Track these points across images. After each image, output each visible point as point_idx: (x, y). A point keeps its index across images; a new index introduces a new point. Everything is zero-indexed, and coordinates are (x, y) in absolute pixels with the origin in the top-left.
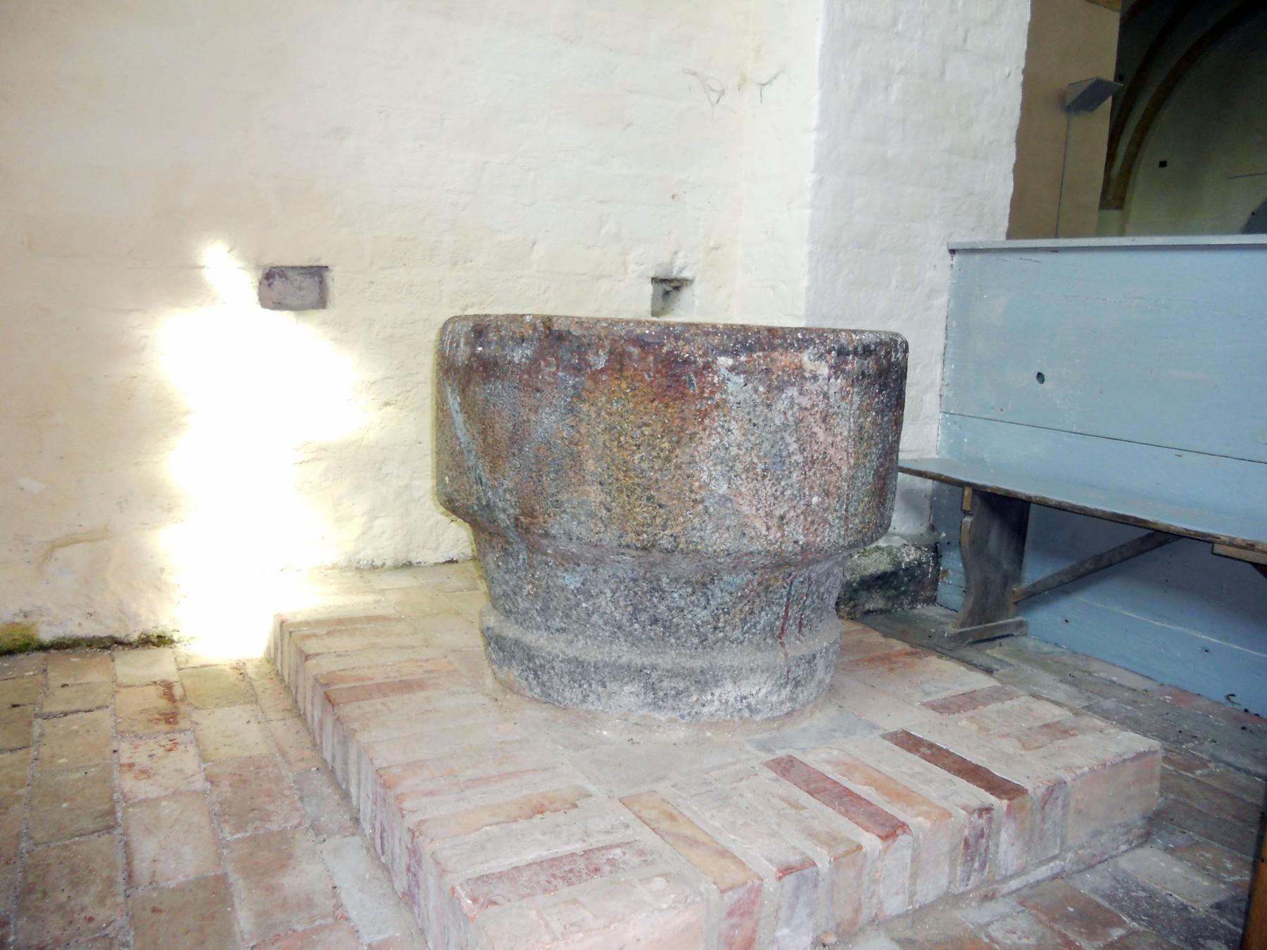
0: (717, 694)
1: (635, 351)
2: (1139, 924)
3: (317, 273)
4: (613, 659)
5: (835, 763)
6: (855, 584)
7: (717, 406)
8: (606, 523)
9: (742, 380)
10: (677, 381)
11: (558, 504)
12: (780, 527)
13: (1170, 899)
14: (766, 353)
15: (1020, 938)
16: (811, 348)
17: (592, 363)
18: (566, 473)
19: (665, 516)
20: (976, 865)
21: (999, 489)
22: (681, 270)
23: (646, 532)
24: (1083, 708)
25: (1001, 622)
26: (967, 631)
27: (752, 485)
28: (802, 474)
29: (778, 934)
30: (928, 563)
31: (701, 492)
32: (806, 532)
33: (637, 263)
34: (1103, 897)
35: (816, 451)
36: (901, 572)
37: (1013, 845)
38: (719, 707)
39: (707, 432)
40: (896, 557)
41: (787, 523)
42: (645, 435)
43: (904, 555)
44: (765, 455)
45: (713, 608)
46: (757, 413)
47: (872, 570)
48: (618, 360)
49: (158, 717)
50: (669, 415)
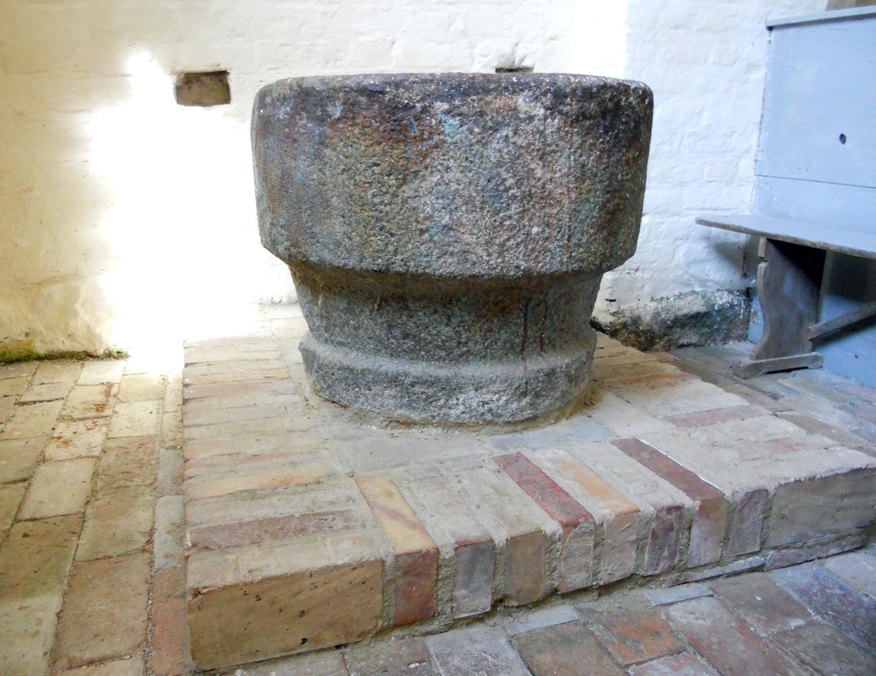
0: (461, 400)
1: (363, 99)
2: (823, 618)
3: (220, 76)
4: (375, 367)
5: (551, 460)
6: (669, 322)
7: (436, 147)
8: (349, 250)
9: (457, 122)
10: (399, 125)
11: (313, 235)
12: (500, 254)
13: (865, 599)
14: (480, 96)
15: (697, 619)
16: (526, 91)
17: (331, 114)
18: (317, 209)
19: (395, 244)
20: (666, 553)
21: (789, 237)
22: (522, 61)
23: (379, 257)
24: (851, 431)
25: (792, 357)
26: (761, 363)
27: (471, 216)
28: (520, 207)
29: (457, 593)
30: (739, 305)
31: (426, 222)
32: (526, 258)
33: (482, 56)
34: (796, 591)
35: (534, 186)
36: (715, 313)
37: (706, 539)
38: (464, 410)
39: (429, 170)
40: (710, 300)
41: (507, 250)
42: (375, 174)
43: (718, 298)
44: (483, 190)
45: (454, 326)
46: (473, 152)
47: (685, 311)
48: (350, 106)
49: (92, 406)
50: (394, 156)
